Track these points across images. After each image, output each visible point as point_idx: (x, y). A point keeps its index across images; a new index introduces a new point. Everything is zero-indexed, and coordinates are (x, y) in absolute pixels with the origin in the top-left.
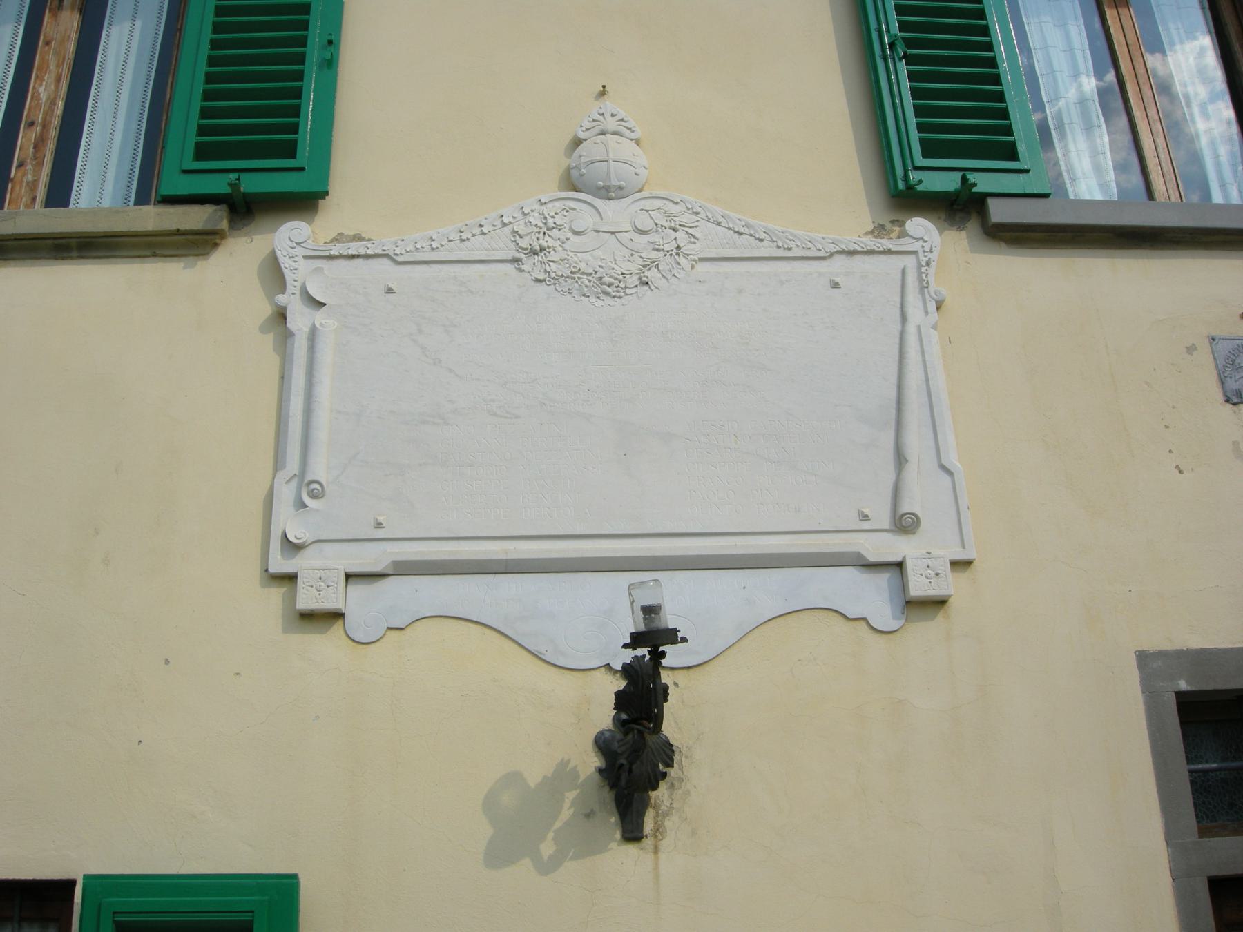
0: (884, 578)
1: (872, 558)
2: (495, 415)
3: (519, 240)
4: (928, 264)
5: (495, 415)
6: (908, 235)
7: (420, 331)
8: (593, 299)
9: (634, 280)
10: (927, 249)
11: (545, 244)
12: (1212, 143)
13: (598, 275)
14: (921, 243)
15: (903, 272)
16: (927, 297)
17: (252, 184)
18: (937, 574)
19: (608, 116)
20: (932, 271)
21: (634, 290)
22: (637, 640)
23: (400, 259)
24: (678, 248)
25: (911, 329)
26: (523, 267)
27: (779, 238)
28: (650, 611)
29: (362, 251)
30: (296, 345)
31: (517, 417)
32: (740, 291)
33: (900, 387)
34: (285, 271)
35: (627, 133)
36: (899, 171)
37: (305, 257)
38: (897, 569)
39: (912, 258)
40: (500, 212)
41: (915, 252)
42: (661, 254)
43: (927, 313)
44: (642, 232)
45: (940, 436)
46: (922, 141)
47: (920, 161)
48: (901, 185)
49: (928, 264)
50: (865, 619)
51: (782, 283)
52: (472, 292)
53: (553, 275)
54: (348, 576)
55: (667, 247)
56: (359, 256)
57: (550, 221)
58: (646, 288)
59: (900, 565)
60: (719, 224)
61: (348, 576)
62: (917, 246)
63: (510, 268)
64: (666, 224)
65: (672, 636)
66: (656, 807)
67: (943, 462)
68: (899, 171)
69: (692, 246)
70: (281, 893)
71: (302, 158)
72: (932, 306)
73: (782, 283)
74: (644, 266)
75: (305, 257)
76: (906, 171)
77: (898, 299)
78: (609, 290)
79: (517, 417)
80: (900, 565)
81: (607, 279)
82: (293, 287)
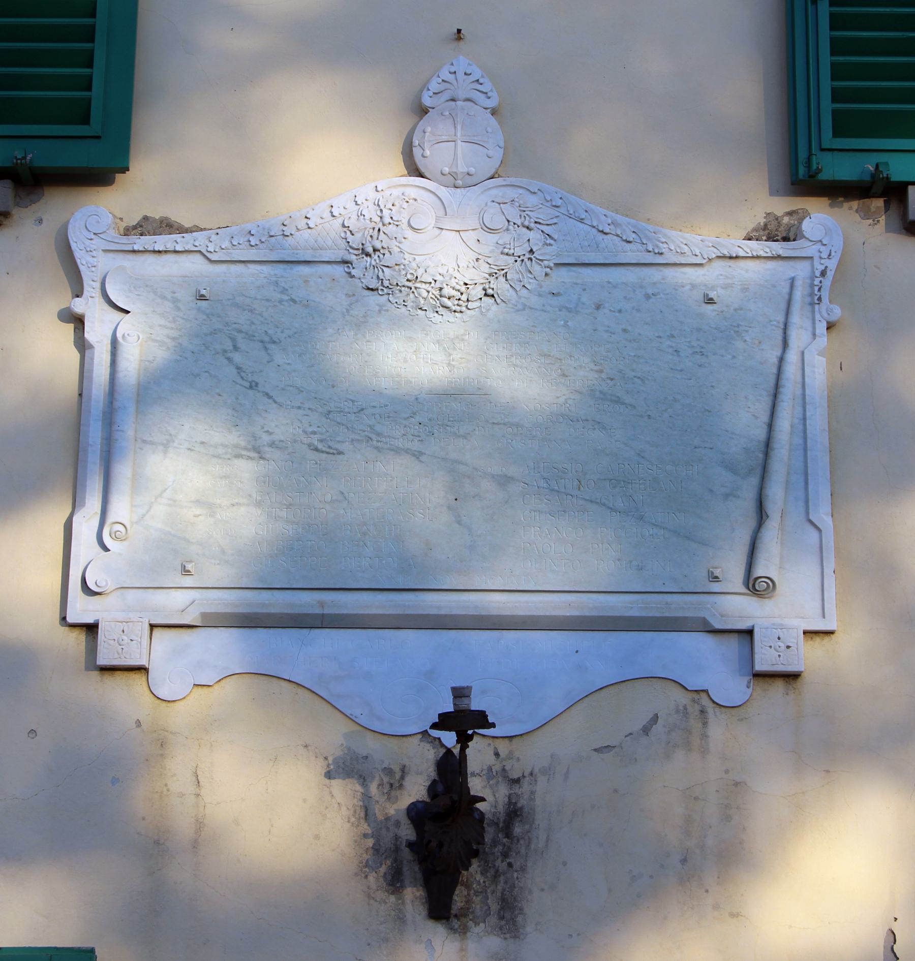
0: (734, 640)
1: (718, 626)
2: (317, 450)
3: (350, 238)
4: (823, 274)
5: (317, 450)
6: (803, 237)
7: (235, 348)
8: (430, 314)
9: (478, 292)
10: (825, 255)
11: (378, 245)
12: (685, 274)
13: (438, 285)
14: (818, 246)
15: (792, 281)
16: (817, 316)
17: (40, 155)
18: (788, 647)
19: (460, 75)
20: (827, 282)
21: (477, 304)
22: (444, 722)
23: (214, 257)
24: (531, 251)
25: (792, 357)
26: (353, 272)
27: (649, 239)
28: (460, 693)
29: (170, 247)
30: (96, 361)
31: (340, 453)
32: (598, 307)
33: (770, 426)
34: (81, 268)
35: (480, 98)
36: (802, 155)
37: (105, 251)
38: (748, 638)
39: (806, 265)
40: (329, 202)
41: (811, 258)
42: (511, 260)
43: (814, 335)
44: (491, 230)
45: (810, 487)
46: (835, 113)
47: (828, 139)
48: (802, 171)
49: (823, 274)
50: (706, 691)
51: (648, 297)
52: (294, 301)
53: (386, 283)
54: (152, 627)
55: (518, 252)
56: (166, 252)
57: (386, 213)
58: (491, 300)
59: (750, 633)
60: (581, 220)
61: (152, 627)
62: (811, 250)
63: (340, 270)
64: (519, 222)
65: (481, 720)
66: (468, 886)
67: (811, 518)
68: (802, 155)
69: (549, 249)
70: (92, 951)
71: (94, 127)
72: (821, 327)
73: (648, 297)
74: (490, 275)
75: (105, 251)
76: (810, 155)
77: (781, 318)
78: (448, 303)
79: (340, 453)
80: (750, 633)
81: (447, 291)
82: (91, 288)
